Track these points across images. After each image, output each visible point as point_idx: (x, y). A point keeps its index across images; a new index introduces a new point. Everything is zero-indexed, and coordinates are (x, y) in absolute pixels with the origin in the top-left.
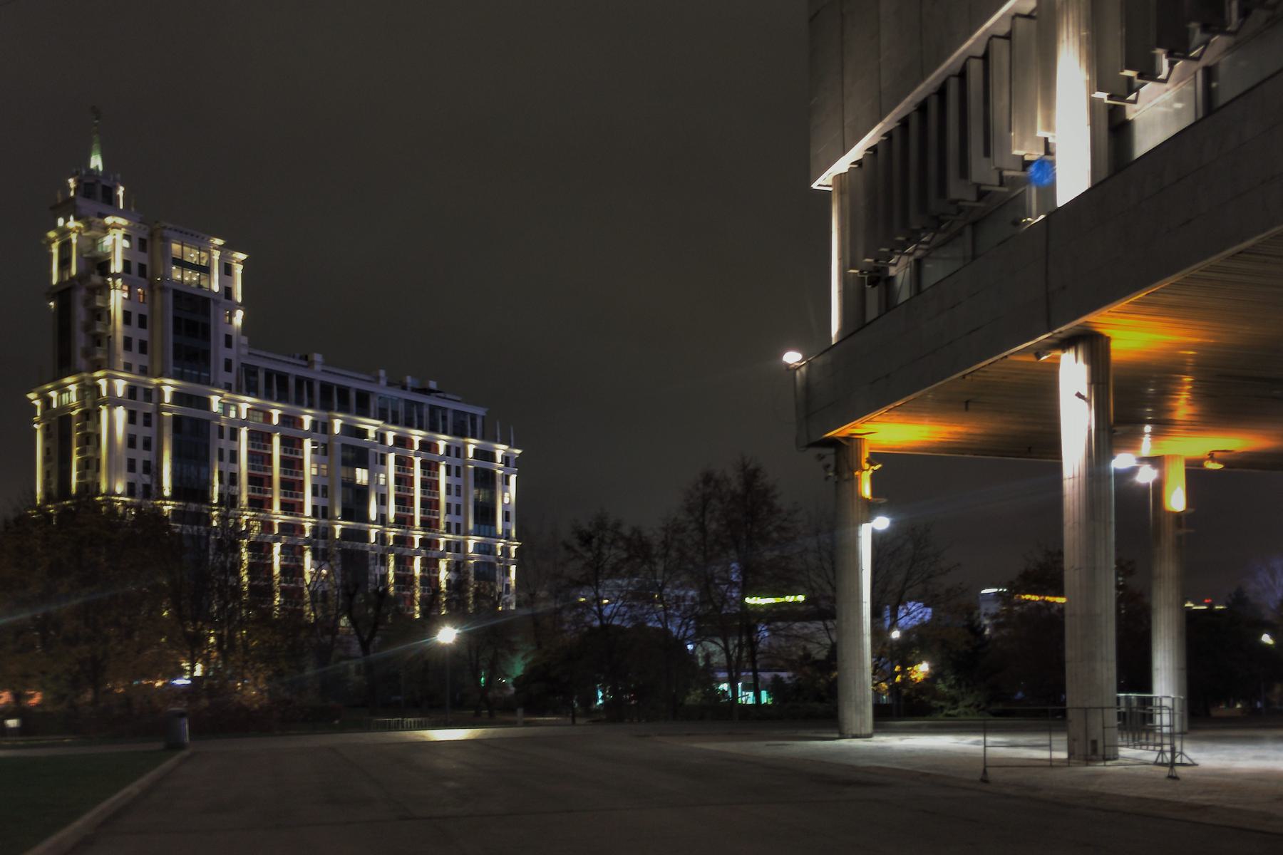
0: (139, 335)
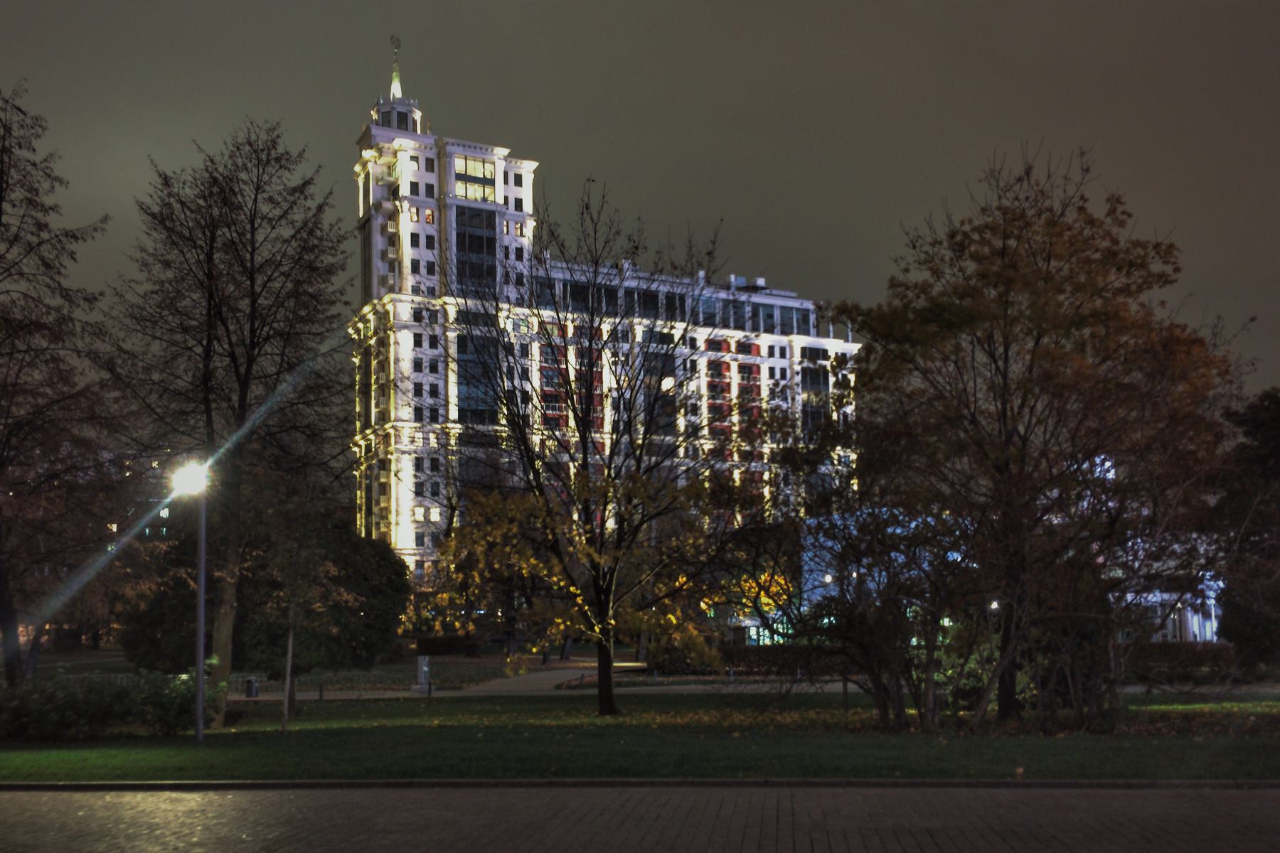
0: (427, 255)
